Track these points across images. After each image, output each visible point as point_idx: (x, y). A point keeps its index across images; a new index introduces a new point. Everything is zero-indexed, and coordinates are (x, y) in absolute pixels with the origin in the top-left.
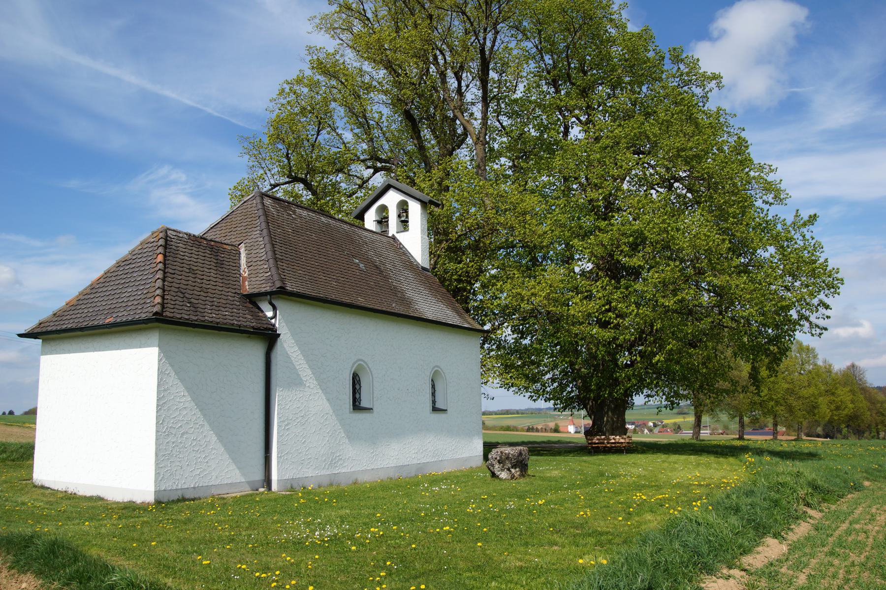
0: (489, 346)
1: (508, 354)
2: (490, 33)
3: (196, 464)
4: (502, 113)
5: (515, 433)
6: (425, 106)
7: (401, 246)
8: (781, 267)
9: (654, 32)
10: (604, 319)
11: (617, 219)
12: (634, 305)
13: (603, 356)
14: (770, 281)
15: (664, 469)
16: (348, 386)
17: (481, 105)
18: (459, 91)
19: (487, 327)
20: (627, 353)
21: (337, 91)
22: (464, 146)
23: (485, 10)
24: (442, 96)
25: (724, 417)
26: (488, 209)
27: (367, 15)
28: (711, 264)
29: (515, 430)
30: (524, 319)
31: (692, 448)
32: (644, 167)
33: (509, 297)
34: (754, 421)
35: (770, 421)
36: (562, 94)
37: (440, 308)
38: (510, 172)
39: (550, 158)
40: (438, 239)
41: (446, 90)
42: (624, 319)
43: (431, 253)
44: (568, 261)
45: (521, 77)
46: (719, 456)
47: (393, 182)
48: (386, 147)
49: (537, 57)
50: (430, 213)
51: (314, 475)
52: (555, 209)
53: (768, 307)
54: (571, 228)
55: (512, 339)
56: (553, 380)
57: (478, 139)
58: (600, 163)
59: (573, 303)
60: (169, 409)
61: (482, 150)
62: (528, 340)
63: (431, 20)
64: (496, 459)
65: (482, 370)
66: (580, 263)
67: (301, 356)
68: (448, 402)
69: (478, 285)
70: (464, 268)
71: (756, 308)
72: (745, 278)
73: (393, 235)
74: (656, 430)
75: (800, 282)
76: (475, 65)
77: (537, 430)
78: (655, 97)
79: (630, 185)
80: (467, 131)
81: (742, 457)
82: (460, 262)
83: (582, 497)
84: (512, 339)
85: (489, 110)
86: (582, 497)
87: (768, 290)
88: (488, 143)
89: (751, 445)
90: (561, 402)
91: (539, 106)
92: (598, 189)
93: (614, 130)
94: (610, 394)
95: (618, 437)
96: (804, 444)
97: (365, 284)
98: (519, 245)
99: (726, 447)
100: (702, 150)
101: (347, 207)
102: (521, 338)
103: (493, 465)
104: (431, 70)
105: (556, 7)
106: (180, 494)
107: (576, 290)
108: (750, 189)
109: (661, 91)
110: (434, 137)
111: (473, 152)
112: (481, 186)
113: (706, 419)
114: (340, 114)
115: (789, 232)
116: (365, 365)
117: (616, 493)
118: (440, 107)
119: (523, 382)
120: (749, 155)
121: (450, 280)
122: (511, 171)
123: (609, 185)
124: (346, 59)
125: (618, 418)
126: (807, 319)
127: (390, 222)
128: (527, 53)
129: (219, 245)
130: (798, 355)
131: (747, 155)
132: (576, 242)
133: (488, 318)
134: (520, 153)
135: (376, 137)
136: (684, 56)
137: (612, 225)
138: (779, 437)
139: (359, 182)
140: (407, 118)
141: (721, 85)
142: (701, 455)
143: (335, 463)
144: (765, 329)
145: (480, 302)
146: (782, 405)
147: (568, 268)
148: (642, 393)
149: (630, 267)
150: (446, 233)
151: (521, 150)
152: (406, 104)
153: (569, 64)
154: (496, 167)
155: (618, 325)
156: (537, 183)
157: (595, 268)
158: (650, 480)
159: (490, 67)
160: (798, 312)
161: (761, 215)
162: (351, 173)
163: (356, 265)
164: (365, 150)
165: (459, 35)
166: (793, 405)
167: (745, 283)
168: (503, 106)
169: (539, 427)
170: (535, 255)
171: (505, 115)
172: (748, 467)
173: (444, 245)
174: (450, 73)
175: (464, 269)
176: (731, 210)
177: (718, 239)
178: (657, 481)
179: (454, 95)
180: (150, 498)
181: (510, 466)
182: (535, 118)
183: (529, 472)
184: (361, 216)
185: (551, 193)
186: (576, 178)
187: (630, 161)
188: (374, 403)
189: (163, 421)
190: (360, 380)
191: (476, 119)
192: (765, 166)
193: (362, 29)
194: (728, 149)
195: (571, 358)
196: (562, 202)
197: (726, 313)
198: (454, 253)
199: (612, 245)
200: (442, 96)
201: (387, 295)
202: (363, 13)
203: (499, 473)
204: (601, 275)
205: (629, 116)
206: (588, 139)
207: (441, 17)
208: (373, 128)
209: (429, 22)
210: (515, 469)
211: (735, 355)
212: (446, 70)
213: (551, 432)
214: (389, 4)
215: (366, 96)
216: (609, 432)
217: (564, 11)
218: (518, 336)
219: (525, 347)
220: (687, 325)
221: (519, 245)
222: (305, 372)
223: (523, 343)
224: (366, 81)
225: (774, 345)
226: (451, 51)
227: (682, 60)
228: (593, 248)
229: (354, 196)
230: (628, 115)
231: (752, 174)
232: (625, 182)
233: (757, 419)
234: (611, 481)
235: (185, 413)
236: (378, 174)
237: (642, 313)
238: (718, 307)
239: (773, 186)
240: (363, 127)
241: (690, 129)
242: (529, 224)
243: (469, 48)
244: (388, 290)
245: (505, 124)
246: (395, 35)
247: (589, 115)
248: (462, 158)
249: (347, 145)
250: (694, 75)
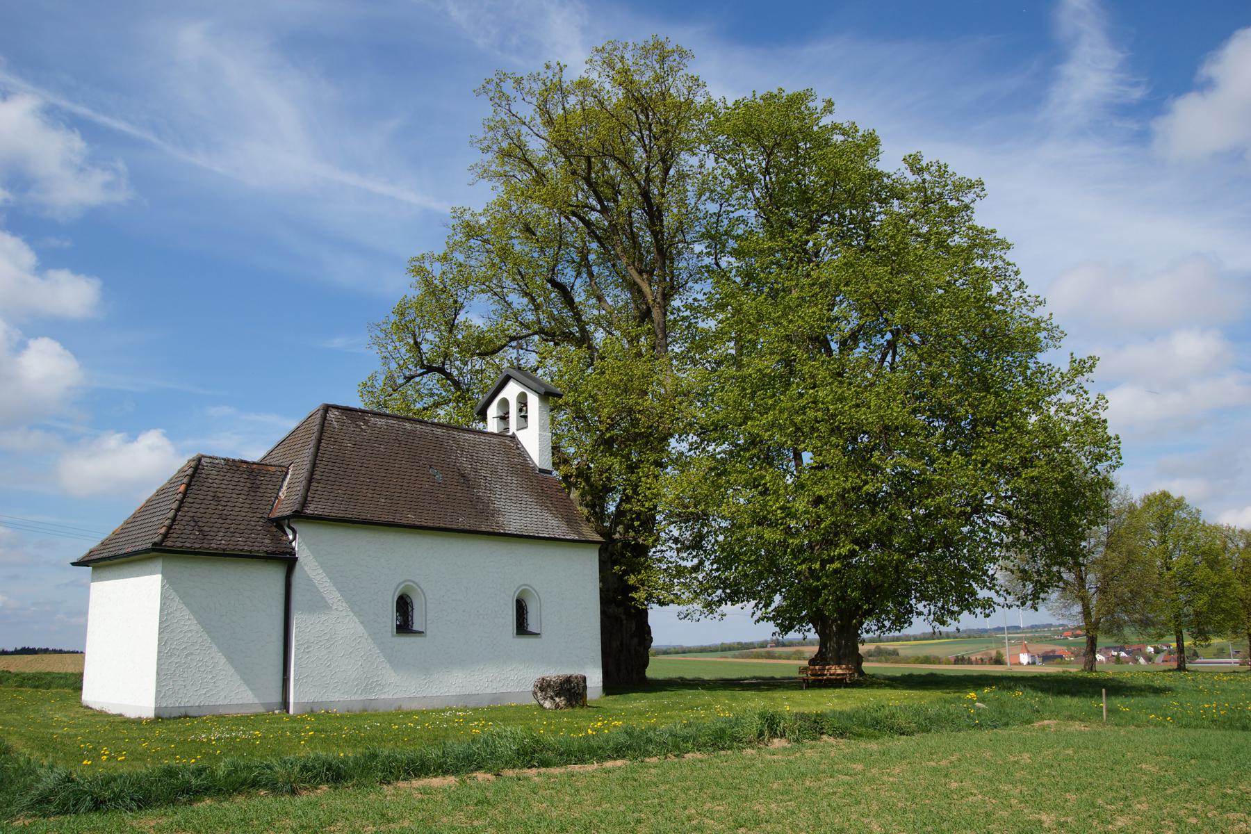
5: (772, 661)
7: (519, 446)
16: (511, 606)
60: (172, 631)
73: (514, 433)
77: (970, 662)
106: (183, 711)
116: (414, 585)
129: (261, 467)
169: (973, 658)
210: (560, 697)
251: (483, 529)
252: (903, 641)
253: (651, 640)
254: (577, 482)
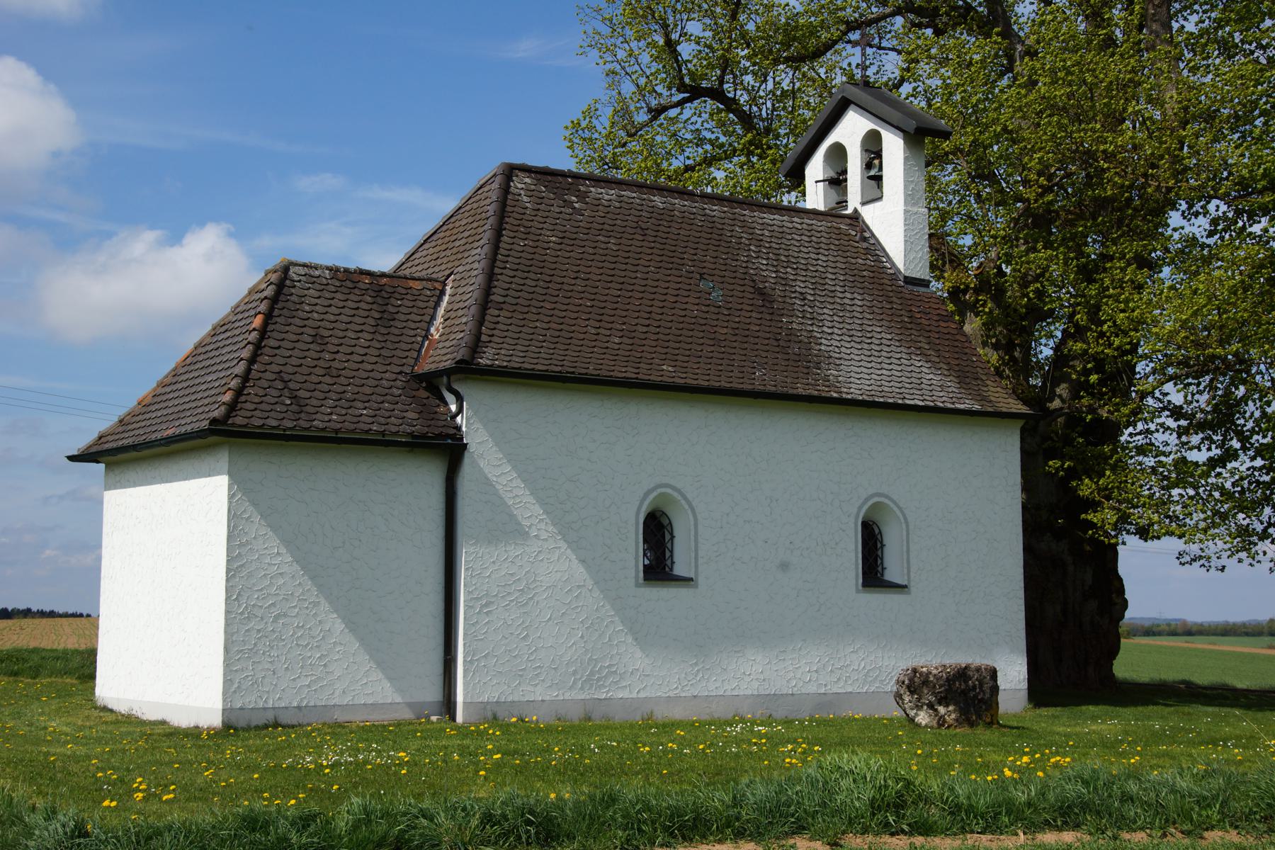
3: (302, 667)
7: (867, 235)
51: (548, 698)
60: (250, 575)
67: (519, 480)
73: (856, 210)
106: (270, 716)
116: (675, 494)
129: (396, 282)
143: (598, 680)
180: (216, 720)
188: (700, 569)
189: (239, 595)
210: (947, 706)
222: (528, 510)
235: (281, 581)
251: (800, 391)
253: (1125, 604)
254: (977, 301)
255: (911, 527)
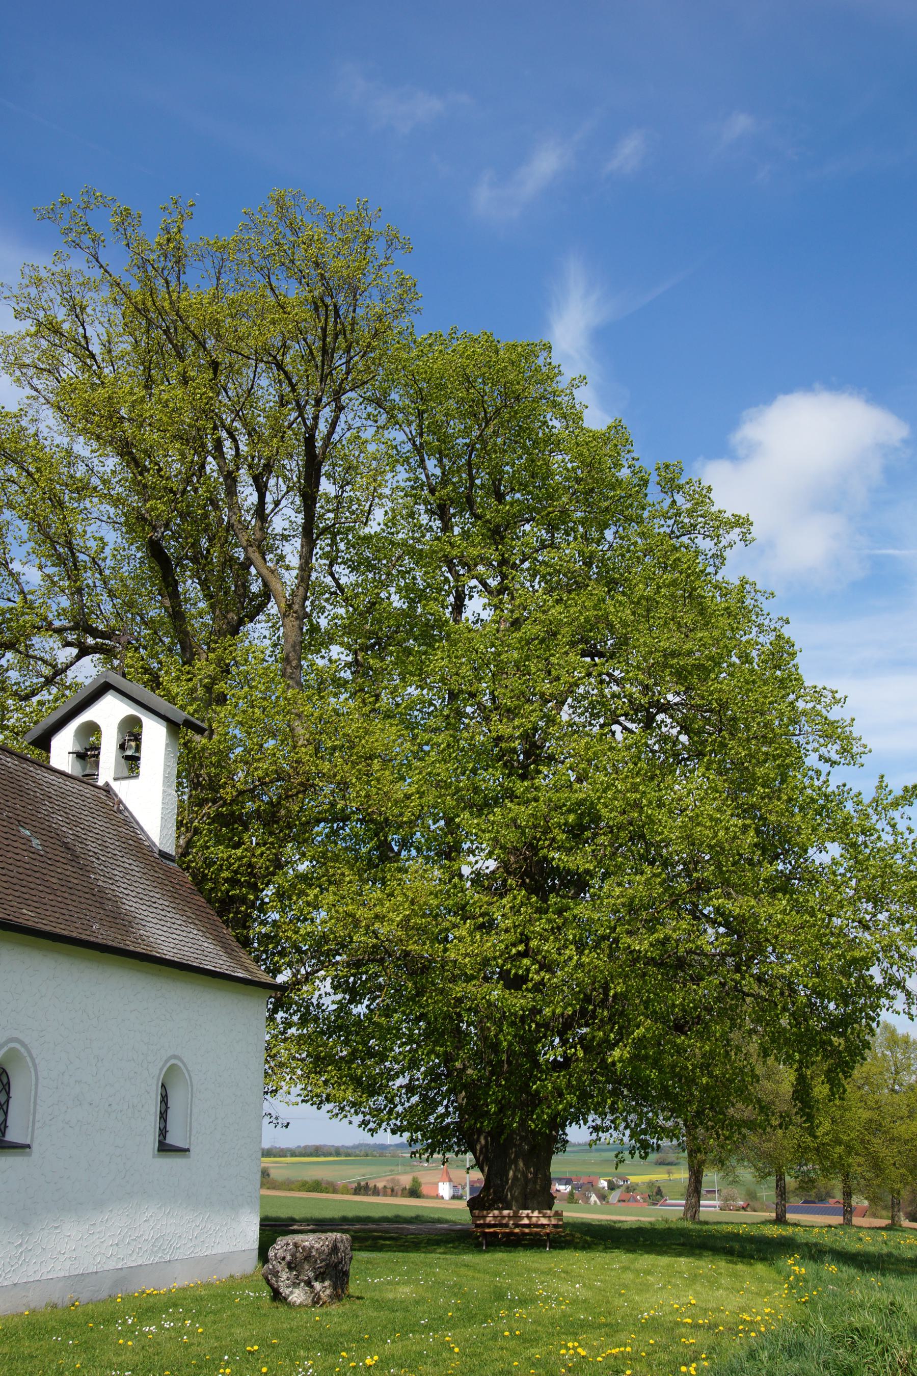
0: (285, 1015)
1: (323, 1033)
2: (328, 409)
4: (340, 560)
6: (192, 536)
7: (122, 807)
8: (853, 883)
9: (633, 431)
10: (513, 972)
11: (546, 778)
12: (572, 947)
13: (510, 1044)
14: (831, 910)
15: (626, 1286)
17: (299, 541)
18: (260, 511)
19: (281, 979)
20: (557, 1040)
21: (17, 488)
22: (261, 617)
23: (319, 364)
24: (226, 519)
25: (746, 1174)
26: (300, 743)
27: (90, 349)
28: (721, 872)
29: (331, 1190)
30: (358, 964)
31: (682, 1240)
32: (602, 682)
33: (330, 919)
34: (807, 1184)
35: (837, 1185)
36: (456, 533)
37: (191, 935)
38: (347, 675)
39: (425, 653)
40: (197, 796)
41: (234, 507)
42: (554, 973)
43: (180, 824)
44: (450, 853)
45: (381, 496)
46: (735, 1259)
47: (115, 679)
48: (107, 607)
49: (411, 460)
50: (185, 744)
52: (429, 752)
53: (828, 958)
54: (458, 790)
55: (333, 1002)
56: (410, 1089)
57: (290, 606)
58: (518, 669)
59: (455, 938)
61: (296, 629)
62: (364, 1006)
63: (215, 373)
64: (284, 1258)
65: (267, 1066)
66: (471, 858)
68: (194, 1132)
69: (270, 891)
70: (246, 856)
71: (804, 961)
72: (784, 902)
73: (107, 784)
74: (614, 1197)
75: (886, 914)
76: (294, 466)
77: (376, 1192)
78: (629, 551)
79: (574, 713)
80: (270, 591)
81: (781, 1263)
82: (237, 846)
83: (457, 1350)
84: (333, 1002)
85: (314, 552)
86: (457, 1350)
87: (827, 927)
88: (308, 616)
89: (801, 1235)
90: (423, 1135)
91: (411, 551)
92: (513, 719)
93: (549, 610)
94: (522, 1122)
95: (536, 1214)
96: (905, 1239)
97: (38, 882)
98: (356, 817)
99: (751, 1239)
100: (711, 658)
101: (18, 720)
102: (350, 1002)
103: (276, 1274)
104: (208, 468)
105: (454, 371)
107: (462, 911)
108: (797, 732)
109: (639, 541)
110: (205, 596)
111: (278, 629)
112: (290, 699)
113: (711, 1177)
114: (18, 534)
115: (867, 817)
116: (22, 1050)
117: (525, 1341)
118: (220, 538)
119: (349, 1093)
120: (797, 669)
121: (216, 881)
122: (349, 672)
123: (533, 711)
124: (42, 426)
125: (535, 1174)
126: (900, 985)
127: (102, 758)
128: (395, 452)
130: (888, 1053)
131: (793, 669)
132: (465, 818)
133: (287, 959)
134: (370, 639)
135: (88, 586)
136: (682, 481)
137: (537, 789)
138: (856, 1221)
139: (47, 671)
140: (153, 556)
141: (749, 537)
142: (700, 1256)
144: (822, 1003)
145: (273, 926)
146: (859, 1155)
147: (449, 867)
148: (586, 1122)
149: (568, 871)
150: (213, 785)
151: (370, 634)
152: (154, 529)
153: (472, 478)
154: (320, 663)
155: (542, 982)
156: (398, 699)
157: (501, 870)
158: (597, 1310)
159: (323, 471)
160: (884, 971)
161: (816, 783)
162: (31, 653)
163: (23, 841)
164: (64, 610)
165: (267, 405)
166: (881, 1155)
167: (784, 912)
168: (342, 546)
169: (380, 1185)
170: (386, 837)
171: (345, 564)
172: (792, 1288)
173: (209, 809)
174: (244, 475)
175: (245, 860)
176: (760, 771)
177: (736, 826)
178: (610, 1313)
179: (249, 518)
181: (311, 1274)
182: (402, 574)
183: (353, 1288)
184: (43, 742)
185: (423, 719)
186: (472, 695)
187: (575, 669)
188: (36, 1132)
190: (9, 1083)
191: (288, 568)
192: (825, 692)
193: (79, 374)
194: (759, 655)
195: (447, 1046)
196: (442, 738)
197: (749, 967)
198: (226, 827)
199: (535, 827)
200: (226, 519)
201: (84, 906)
202: (83, 342)
203: (287, 1291)
204: (511, 885)
205: (578, 585)
206: (498, 622)
207: (236, 367)
208: (85, 568)
209: (211, 376)
210: (323, 1281)
211: (765, 1052)
212: (238, 469)
213: (403, 1196)
214: (137, 333)
215: (76, 505)
216: (517, 1201)
217: (468, 381)
218: (344, 998)
219: (358, 1023)
220: (673, 989)
221: (356, 817)
223: (355, 1011)
224: (78, 475)
225: (841, 1035)
226: (250, 435)
227: (680, 488)
228: (498, 832)
229: (35, 700)
230: (576, 582)
231: (801, 705)
232: (566, 707)
233: (812, 1181)
234: (519, 1312)
236: (86, 660)
237: (589, 964)
238: (733, 955)
239: (839, 730)
240: (65, 564)
241: (688, 618)
242: (378, 780)
243: (285, 432)
244: (87, 896)
245: (343, 581)
246: (143, 393)
247: (504, 577)
248: (256, 641)
249: (29, 597)
250: (701, 516)
252: (275, 1156)
255: (194, 1090)
